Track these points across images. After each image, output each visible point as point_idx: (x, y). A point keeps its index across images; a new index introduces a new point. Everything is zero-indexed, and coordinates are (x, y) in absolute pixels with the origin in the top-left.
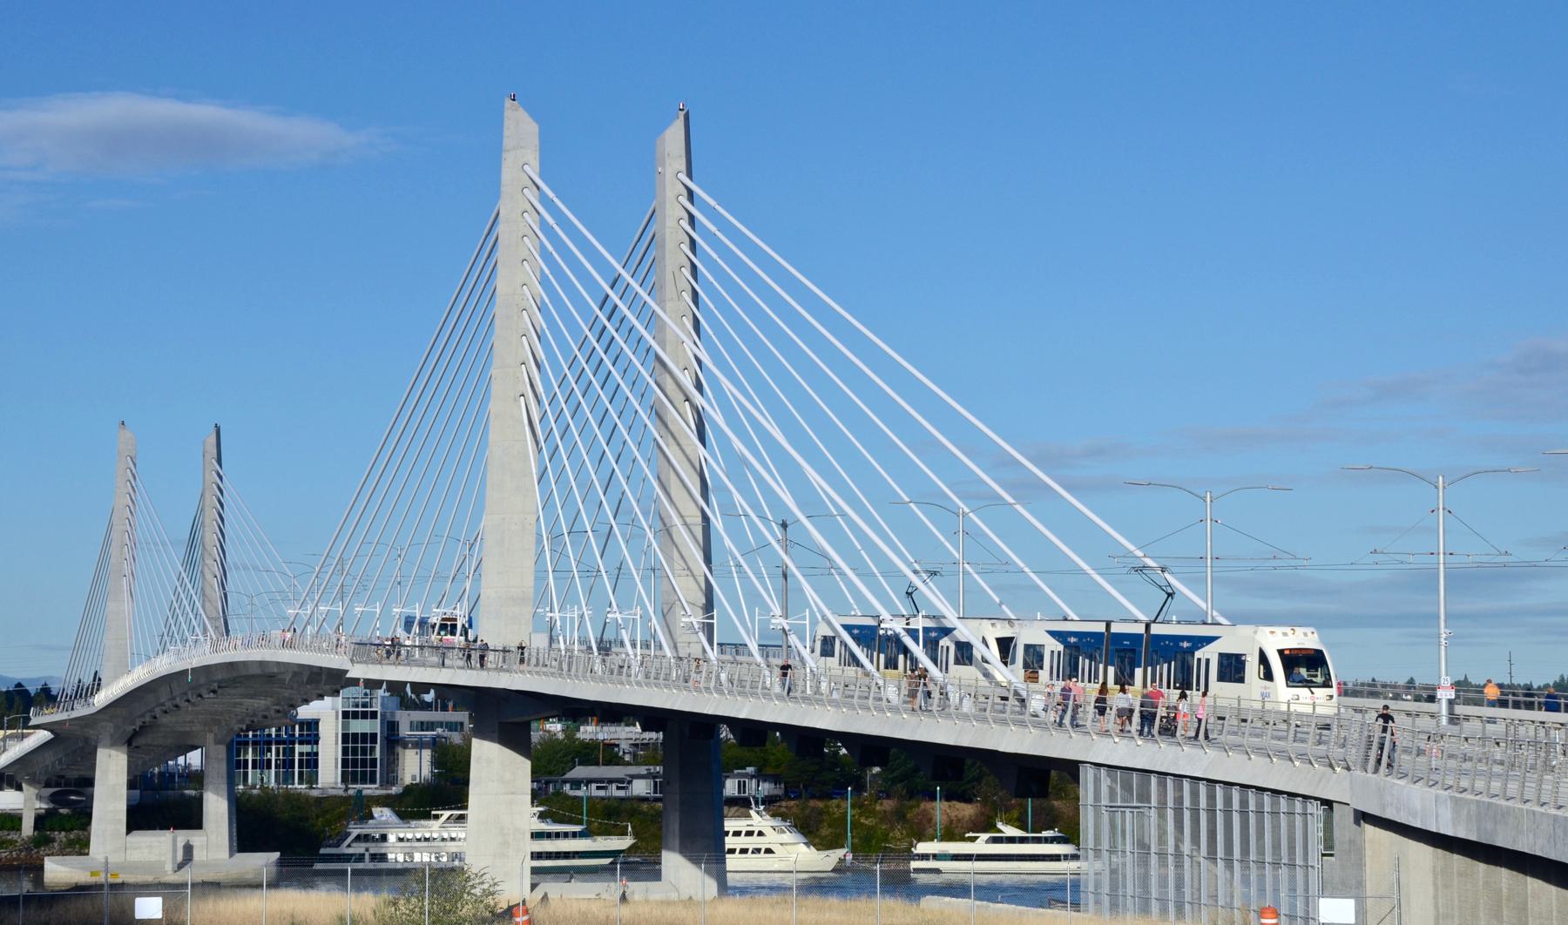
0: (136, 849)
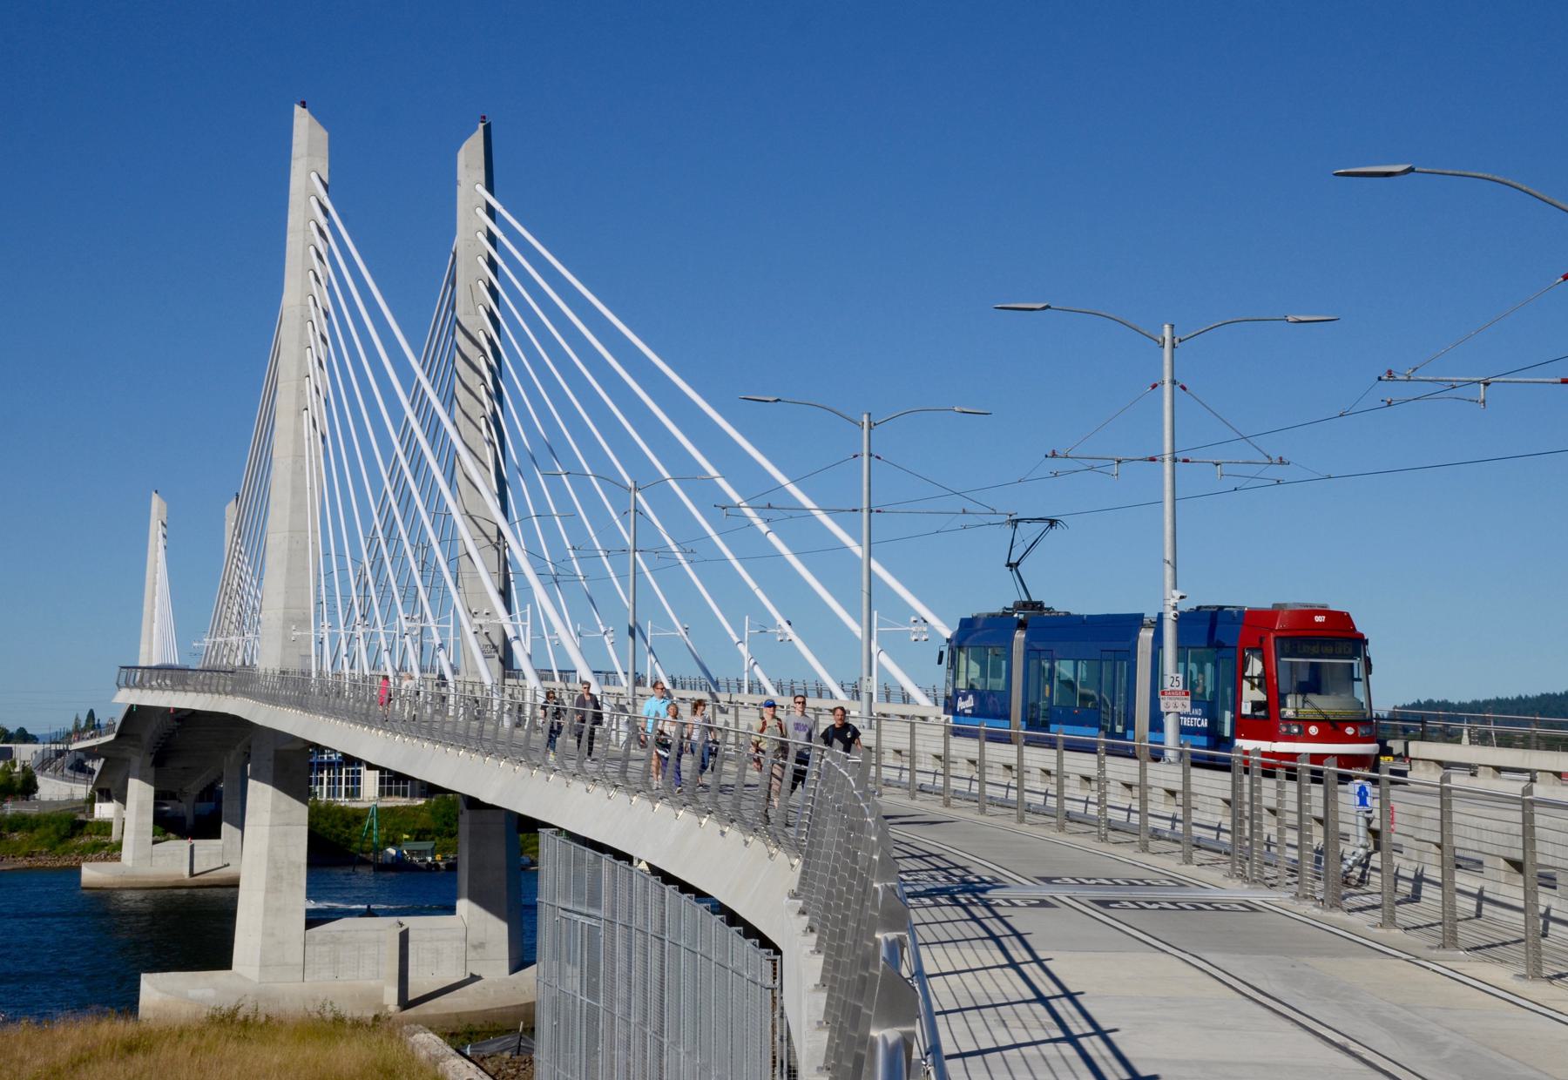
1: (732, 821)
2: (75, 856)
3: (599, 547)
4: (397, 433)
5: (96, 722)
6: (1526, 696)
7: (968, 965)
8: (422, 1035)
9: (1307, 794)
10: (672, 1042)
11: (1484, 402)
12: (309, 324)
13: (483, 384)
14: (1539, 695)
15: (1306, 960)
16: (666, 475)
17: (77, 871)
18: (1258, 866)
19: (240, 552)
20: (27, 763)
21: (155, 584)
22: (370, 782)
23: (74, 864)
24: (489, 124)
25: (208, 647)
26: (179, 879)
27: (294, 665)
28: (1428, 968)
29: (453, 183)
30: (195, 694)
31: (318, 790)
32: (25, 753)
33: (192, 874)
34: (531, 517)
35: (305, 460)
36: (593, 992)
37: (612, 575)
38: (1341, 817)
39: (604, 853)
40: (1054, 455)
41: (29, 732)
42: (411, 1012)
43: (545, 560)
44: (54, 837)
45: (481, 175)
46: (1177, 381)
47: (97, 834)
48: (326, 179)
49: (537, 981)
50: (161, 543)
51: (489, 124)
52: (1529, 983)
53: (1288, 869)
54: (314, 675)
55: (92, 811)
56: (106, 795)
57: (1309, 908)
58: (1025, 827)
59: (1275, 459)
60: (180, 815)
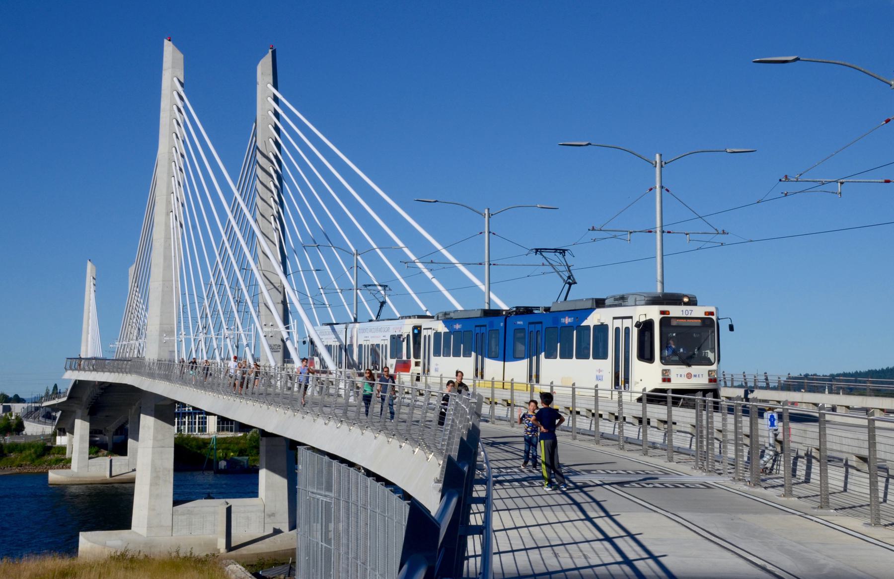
0: (93, 466)
1: (394, 435)
2: (45, 466)
3: (337, 287)
4: (224, 229)
5: (58, 391)
6: (860, 371)
7: (548, 521)
8: (234, 565)
9: (740, 425)
10: (372, 569)
11: (840, 193)
12: (173, 163)
13: (272, 197)
14: (867, 370)
15: (740, 516)
16: (375, 246)
17: (46, 475)
18: (711, 462)
19: (136, 291)
20: (18, 414)
21: (89, 312)
22: (212, 424)
23: (45, 471)
24: (275, 50)
25: (118, 347)
26: (103, 478)
27: (166, 356)
28: (812, 520)
29: (254, 83)
30: (109, 373)
31: (182, 428)
32: (18, 409)
33: (111, 476)
34: (300, 271)
35: (171, 240)
36: (328, 541)
37: (345, 304)
38: (760, 433)
39: (334, 459)
40: (593, 229)
41: (21, 397)
42: (233, 553)
43: (307, 296)
44: (34, 456)
45: (270, 79)
46: (664, 186)
47: (58, 454)
48: (182, 81)
49: (297, 534)
50: (93, 288)
51: (275, 50)
52: (873, 528)
53: (729, 464)
54: (176, 362)
55: (55, 441)
56: (62, 431)
57: (741, 486)
58: (576, 442)
59: (720, 231)
60: (105, 443)
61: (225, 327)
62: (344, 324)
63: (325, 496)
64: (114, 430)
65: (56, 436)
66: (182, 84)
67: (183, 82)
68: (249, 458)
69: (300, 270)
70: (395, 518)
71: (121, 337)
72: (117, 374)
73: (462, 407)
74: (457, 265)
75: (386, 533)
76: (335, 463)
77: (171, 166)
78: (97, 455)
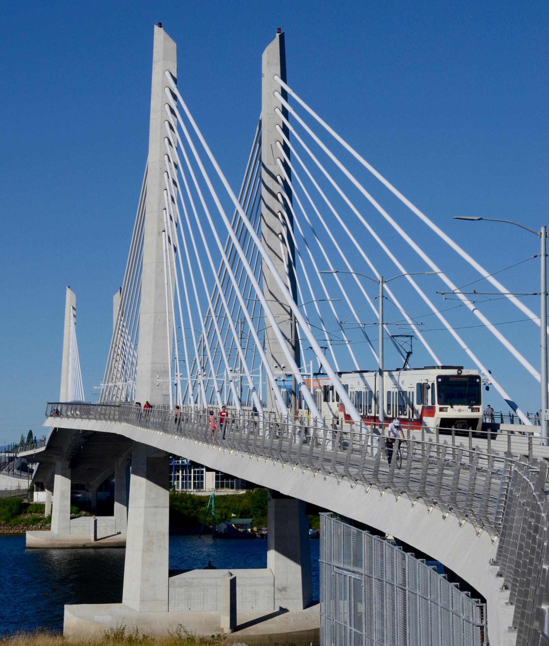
2: (22, 527)
16: (404, 272)
21: (69, 348)
23: (21, 532)
25: (103, 389)
33: (96, 539)
39: (363, 529)
42: (239, 633)
44: (9, 514)
45: (277, 69)
47: (36, 512)
48: (175, 75)
50: (72, 320)
55: (32, 497)
56: (40, 487)
61: (228, 369)
62: (373, 372)
63: (354, 572)
64: (98, 485)
65: (34, 491)
66: (175, 80)
67: (176, 78)
68: (253, 520)
69: (314, 299)
70: (439, 603)
71: (106, 378)
72: (104, 422)
73: (524, 479)
74: (508, 296)
75: (430, 619)
76: (365, 534)
77: (163, 177)
78: (79, 515)
